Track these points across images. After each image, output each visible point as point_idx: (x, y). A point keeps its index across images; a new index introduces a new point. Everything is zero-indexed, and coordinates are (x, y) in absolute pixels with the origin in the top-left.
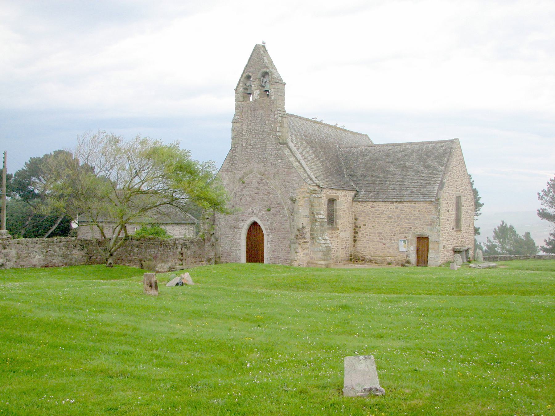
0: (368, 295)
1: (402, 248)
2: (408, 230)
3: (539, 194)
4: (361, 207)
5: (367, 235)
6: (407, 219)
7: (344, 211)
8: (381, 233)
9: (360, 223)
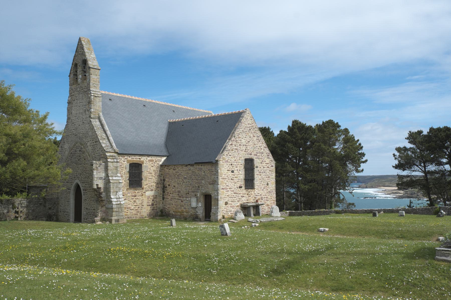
0: (281, 232)
1: (194, 204)
2: (197, 189)
3: (394, 155)
4: (167, 170)
5: (171, 193)
6: (197, 180)
7: (151, 173)
8: (179, 192)
9: (167, 183)
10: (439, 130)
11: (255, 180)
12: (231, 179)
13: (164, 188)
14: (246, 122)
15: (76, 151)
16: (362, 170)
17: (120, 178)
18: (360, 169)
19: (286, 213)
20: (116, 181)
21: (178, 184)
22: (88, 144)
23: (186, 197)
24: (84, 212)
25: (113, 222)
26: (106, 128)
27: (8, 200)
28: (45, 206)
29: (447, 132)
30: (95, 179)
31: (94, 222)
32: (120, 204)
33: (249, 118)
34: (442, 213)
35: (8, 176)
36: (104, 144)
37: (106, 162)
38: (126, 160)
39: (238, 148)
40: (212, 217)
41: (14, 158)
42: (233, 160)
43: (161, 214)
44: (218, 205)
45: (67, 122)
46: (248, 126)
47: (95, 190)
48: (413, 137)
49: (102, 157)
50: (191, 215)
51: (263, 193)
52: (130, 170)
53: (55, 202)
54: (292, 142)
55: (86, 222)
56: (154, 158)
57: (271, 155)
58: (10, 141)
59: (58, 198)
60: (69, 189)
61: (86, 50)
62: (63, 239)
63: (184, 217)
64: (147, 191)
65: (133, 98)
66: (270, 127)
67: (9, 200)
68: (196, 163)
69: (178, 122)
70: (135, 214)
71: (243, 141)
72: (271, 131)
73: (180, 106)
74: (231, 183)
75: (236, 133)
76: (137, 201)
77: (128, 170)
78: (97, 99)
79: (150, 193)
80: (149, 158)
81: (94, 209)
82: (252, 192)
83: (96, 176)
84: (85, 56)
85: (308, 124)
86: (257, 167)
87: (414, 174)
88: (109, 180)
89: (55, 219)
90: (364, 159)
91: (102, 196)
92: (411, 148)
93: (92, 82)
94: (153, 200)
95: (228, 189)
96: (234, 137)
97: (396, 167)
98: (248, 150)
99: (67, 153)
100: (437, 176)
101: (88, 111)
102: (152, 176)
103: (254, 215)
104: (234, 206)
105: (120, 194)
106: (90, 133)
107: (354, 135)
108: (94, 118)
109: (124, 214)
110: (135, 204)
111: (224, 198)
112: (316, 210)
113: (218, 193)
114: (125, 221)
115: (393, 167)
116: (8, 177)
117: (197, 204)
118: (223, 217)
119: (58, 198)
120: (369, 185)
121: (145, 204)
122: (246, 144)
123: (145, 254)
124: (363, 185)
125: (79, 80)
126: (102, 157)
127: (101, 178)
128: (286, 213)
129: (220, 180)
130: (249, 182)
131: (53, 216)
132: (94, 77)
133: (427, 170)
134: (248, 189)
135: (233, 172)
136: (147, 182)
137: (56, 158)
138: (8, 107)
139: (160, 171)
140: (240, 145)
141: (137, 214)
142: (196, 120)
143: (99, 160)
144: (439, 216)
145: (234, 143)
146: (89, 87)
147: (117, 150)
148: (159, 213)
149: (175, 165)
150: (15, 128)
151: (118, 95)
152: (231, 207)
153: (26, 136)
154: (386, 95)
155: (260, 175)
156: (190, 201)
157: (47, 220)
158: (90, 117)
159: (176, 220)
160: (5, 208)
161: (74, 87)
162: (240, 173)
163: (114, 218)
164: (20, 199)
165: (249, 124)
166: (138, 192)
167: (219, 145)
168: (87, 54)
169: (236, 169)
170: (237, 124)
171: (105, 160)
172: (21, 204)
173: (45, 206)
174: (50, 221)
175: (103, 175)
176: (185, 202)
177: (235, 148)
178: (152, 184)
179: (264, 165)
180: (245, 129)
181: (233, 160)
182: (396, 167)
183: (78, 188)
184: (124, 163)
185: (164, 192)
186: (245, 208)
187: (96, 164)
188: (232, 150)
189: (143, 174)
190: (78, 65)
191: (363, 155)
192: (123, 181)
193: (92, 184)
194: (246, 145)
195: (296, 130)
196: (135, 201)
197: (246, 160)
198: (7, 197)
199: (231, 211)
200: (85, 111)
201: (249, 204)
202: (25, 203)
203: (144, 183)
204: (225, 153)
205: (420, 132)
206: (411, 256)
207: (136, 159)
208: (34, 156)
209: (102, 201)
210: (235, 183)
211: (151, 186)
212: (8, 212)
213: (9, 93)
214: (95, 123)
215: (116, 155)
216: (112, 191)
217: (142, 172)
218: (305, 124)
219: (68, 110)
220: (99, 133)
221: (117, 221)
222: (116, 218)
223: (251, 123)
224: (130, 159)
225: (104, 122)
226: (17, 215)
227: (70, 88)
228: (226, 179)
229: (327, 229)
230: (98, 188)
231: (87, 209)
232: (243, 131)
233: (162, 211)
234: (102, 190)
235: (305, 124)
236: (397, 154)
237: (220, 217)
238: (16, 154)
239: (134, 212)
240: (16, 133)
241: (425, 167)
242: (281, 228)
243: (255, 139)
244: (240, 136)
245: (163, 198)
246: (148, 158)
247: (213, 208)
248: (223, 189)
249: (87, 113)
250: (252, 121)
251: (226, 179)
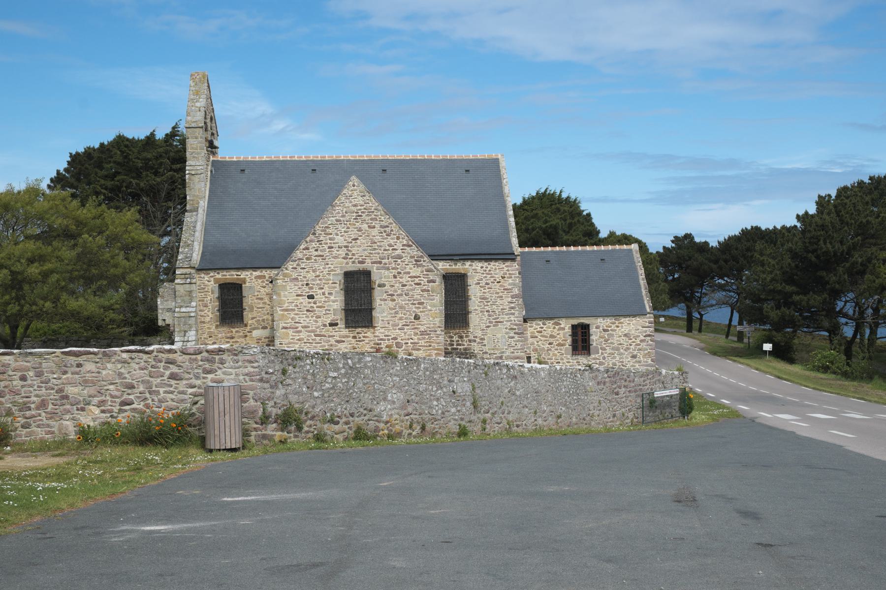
7: (261, 299)
12: (308, 311)
38: (212, 279)
64: (255, 329)
71: (339, 239)
74: (307, 317)
77: (217, 295)
80: (258, 273)
95: (300, 329)
96: (314, 234)
98: (353, 255)
102: (265, 303)
135: (311, 297)
165: (355, 206)
166: (237, 332)
177: (316, 253)
178: (265, 317)
179: (405, 279)
180: (343, 216)
184: (209, 282)
192: (209, 314)
194: (346, 247)
197: (348, 275)
203: (248, 316)
207: (230, 276)
211: (263, 320)
215: (193, 271)
223: (362, 203)
224: (219, 276)
228: (293, 310)
246: (254, 273)
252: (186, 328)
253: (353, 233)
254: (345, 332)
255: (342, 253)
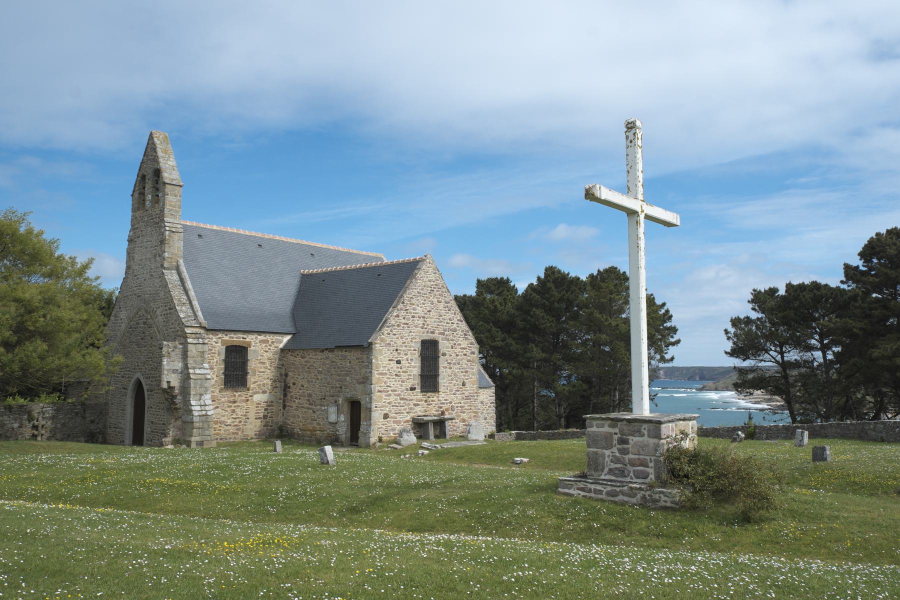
1: (333, 418)
3: (726, 332)
7: (264, 363)
8: (310, 395)
9: (290, 381)
10: (802, 287)
11: (441, 377)
13: (286, 389)
14: (424, 277)
15: (138, 324)
16: (672, 359)
17: (208, 371)
18: (667, 357)
19: (510, 435)
20: (203, 377)
21: (308, 382)
22: (158, 313)
23: (321, 405)
24: (147, 428)
25: (193, 445)
26: (189, 285)
27: (22, 406)
28: (84, 418)
29: (815, 291)
30: (166, 372)
31: (161, 445)
32: (206, 415)
33: (431, 270)
34: (738, 435)
35: (16, 367)
36: (183, 312)
37: (185, 344)
39: (410, 322)
40: (361, 440)
41: (29, 339)
42: (399, 342)
43: (278, 431)
44: (370, 420)
45: (126, 273)
46: (429, 284)
47: (164, 390)
48: (760, 299)
49: (179, 336)
50: (329, 436)
51: (456, 399)
52: (226, 356)
53: (102, 411)
54: (543, 306)
55: (150, 446)
56: (269, 338)
57: (470, 333)
58: (22, 311)
59: (106, 404)
60: (125, 389)
61: (160, 153)
62: (86, 468)
63: (316, 439)
65: (241, 232)
66: (511, 279)
67: (23, 406)
68: (337, 347)
69: (316, 274)
70: (233, 433)
71: (419, 310)
72: (512, 284)
73: (325, 246)
75: (406, 296)
76: (238, 410)
77: (223, 357)
78: (176, 237)
79: (259, 398)
80: (262, 337)
81: (164, 424)
82: (434, 397)
83: (166, 367)
84: (158, 163)
85: (573, 275)
86: (444, 354)
87: (763, 364)
88: (189, 374)
89: (100, 440)
90: (676, 337)
91: (177, 401)
92: (758, 318)
93: (167, 207)
94: (266, 410)
96: (403, 303)
97: (733, 353)
99: (123, 326)
100: (803, 370)
101: (160, 256)
102: (266, 368)
103: (436, 437)
104: (400, 422)
105: (207, 398)
106: (162, 294)
107: (655, 295)
108: (168, 269)
109: (212, 432)
110: (234, 416)
111: (383, 406)
112: (561, 430)
113: (371, 399)
114: (214, 444)
115: (726, 353)
116: (17, 369)
117: (336, 417)
118: (380, 440)
119: (106, 404)
120: (721, 384)
121: (252, 415)
122: (428, 312)
123: (192, 488)
124: (710, 383)
125: (147, 203)
126: (179, 336)
127: (175, 371)
128: (510, 435)
129: (375, 376)
130: (429, 380)
131: (97, 435)
132: (171, 199)
133: (786, 359)
134: (427, 392)
135: (399, 362)
136: (256, 378)
137: (101, 336)
138: (23, 252)
139: (280, 360)
140: (413, 317)
141: (237, 434)
142: (346, 271)
143: (175, 340)
144: (734, 440)
145: (403, 313)
146: (163, 216)
147: (204, 323)
148: (277, 432)
149: (304, 350)
150: (34, 285)
151: (215, 228)
152: (394, 422)
153: (49, 301)
154: (752, 213)
155: (450, 368)
156: (327, 411)
157: (87, 442)
158: (162, 266)
159: (283, 444)
160: (15, 420)
161: (138, 213)
162: (413, 364)
163: (193, 439)
164: (41, 405)
165: (430, 281)
166: (239, 396)
167: (375, 319)
168: (161, 160)
169: (405, 357)
170: (409, 282)
171: (183, 341)
172: (44, 414)
173: (84, 418)
174: (93, 442)
175: (179, 365)
176: (318, 413)
177: (404, 321)
179: (458, 350)
181: (399, 342)
182: (733, 353)
183: (139, 386)
184: (217, 345)
185: (285, 395)
186: (420, 426)
187: (168, 346)
188: (398, 326)
189: (249, 364)
190: (147, 178)
191: (674, 330)
192: (214, 376)
193: (160, 381)
194: (424, 317)
195: (550, 285)
196: (234, 411)
197: (424, 342)
198: (22, 400)
199: (393, 430)
200: (155, 256)
201: (425, 418)
202: (50, 411)
203: (251, 379)
204: (386, 330)
205: (773, 291)
206: (533, 489)
207: (236, 339)
208: (62, 335)
209: (176, 409)
210: (403, 382)
211: (264, 385)
212: (20, 427)
213: (22, 230)
214: (171, 277)
215: (202, 331)
216: (192, 393)
217: (247, 360)
218: (568, 274)
219: (128, 253)
220: (177, 294)
221: (200, 444)
222: (198, 439)
225: (185, 274)
226: (36, 433)
227: (133, 216)
228: (386, 374)
229: (526, 460)
230: (170, 387)
231: (152, 422)
232: (419, 293)
233: (281, 429)
234: (177, 391)
235: (568, 274)
236: (732, 330)
237: (373, 439)
238: (30, 331)
239: (232, 429)
240: (32, 299)
241: (782, 353)
242: (460, 458)
243: (441, 306)
244: (413, 301)
245: (284, 407)
247: (363, 423)
248: (380, 391)
249: (158, 259)
250: (437, 275)
251: (386, 374)
252: (202, 391)
253: (428, 306)
254: (420, 396)
255: (421, 322)
